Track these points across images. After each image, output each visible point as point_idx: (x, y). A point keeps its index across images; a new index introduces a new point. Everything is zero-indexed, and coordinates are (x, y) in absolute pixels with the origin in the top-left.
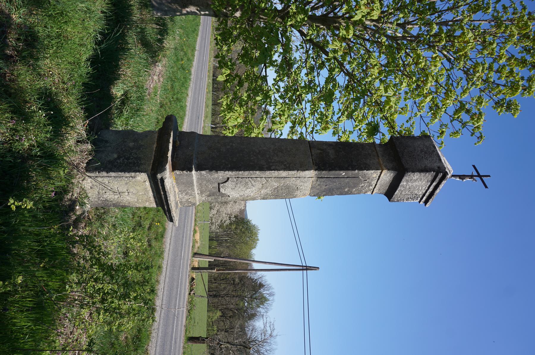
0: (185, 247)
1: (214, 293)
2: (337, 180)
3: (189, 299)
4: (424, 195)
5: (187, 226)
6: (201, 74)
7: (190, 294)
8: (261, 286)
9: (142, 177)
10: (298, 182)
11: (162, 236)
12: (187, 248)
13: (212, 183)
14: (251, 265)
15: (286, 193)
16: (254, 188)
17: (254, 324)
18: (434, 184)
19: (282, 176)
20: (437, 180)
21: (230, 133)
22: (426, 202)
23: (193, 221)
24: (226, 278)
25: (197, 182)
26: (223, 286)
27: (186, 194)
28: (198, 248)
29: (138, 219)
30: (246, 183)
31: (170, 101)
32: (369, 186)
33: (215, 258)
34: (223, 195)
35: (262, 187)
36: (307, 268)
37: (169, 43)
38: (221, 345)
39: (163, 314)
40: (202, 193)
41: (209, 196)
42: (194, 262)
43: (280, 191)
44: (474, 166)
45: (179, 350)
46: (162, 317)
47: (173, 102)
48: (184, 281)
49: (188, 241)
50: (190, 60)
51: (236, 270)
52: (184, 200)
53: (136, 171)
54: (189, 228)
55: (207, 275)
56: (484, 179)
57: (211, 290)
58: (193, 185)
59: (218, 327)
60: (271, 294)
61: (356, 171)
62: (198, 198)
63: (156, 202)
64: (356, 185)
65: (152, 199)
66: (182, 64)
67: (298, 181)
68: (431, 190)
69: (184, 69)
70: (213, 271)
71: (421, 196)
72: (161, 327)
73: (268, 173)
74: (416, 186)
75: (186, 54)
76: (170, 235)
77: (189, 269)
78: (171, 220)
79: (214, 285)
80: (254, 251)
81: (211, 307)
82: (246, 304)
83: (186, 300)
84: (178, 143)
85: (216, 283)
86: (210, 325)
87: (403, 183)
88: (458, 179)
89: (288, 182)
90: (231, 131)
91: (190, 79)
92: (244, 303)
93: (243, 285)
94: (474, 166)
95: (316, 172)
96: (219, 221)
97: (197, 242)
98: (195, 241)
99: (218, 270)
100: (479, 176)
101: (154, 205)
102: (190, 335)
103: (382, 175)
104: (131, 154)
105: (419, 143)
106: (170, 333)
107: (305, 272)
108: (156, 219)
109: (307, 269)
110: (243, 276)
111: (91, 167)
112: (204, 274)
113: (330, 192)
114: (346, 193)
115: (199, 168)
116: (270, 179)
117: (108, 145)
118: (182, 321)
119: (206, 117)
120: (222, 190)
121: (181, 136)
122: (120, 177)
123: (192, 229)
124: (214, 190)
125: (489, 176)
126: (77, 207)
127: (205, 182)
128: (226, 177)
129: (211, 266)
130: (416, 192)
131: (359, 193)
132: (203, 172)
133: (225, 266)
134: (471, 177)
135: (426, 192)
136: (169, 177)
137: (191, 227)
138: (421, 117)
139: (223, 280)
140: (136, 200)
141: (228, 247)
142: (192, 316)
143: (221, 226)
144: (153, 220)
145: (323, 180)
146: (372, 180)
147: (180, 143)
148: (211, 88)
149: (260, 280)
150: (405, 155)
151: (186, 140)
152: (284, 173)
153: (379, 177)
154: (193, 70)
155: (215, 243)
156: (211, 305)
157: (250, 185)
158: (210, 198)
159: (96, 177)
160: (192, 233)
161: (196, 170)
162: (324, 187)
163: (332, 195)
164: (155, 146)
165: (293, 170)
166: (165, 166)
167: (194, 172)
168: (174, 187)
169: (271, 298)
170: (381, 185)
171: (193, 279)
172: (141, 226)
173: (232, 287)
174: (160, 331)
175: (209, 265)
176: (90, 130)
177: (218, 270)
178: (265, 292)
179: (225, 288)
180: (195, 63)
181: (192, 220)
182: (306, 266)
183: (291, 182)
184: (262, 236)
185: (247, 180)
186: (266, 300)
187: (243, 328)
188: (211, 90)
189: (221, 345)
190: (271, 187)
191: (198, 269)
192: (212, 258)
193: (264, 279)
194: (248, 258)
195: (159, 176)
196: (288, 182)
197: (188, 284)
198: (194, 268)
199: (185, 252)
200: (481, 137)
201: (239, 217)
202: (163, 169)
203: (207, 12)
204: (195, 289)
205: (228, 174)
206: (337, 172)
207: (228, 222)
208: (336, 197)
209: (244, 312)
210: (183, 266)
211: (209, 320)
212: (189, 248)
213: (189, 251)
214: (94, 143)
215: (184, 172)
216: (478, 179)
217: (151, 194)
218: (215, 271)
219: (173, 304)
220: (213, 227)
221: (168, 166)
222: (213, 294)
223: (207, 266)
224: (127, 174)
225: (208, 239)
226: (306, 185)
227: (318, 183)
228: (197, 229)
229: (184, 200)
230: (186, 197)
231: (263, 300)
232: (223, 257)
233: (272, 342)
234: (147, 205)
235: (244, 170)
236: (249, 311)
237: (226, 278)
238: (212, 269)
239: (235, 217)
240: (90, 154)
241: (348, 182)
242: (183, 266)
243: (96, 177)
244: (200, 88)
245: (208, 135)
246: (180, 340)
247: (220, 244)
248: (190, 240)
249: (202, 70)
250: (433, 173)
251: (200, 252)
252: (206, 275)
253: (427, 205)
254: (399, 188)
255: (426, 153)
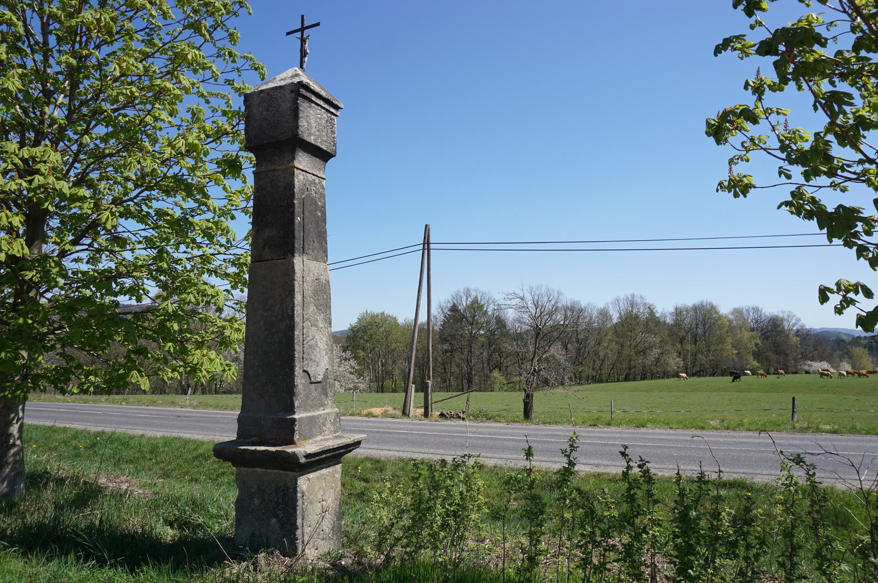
0: (394, 429)
1: (465, 381)
2: (306, 228)
3: (470, 420)
4: (328, 111)
5: (362, 427)
6: (96, 414)
7: (463, 419)
8: (454, 309)
9: (303, 483)
10: (309, 279)
11: (378, 461)
12: (395, 426)
13: (310, 392)
14: (422, 324)
15: (323, 292)
16: (317, 337)
17: (511, 319)
18: (314, 98)
19: (301, 301)
20: (308, 95)
21: (229, 370)
22: (337, 108)
23: (353, 418)
24: (443, 364)
25: (309, 411)
26: (455, 369)
27: (325, 425)
28: (395, 409)
29: (355, 495)
30: (310, 347)
31: (157, 463)
32: (315, 183)
33: (410, 383)
34: (326, 377)
35: (316, 326)
36: (427, 243)
37: (63, 468)
38: (535, 370)
39: (488, 455)
40: (322, 405)
41: (326, 395)
42: (417, 414)
43: (321, 302)
44: (288, 34)
45: (539, 430)
46: (492, 455)
47: (158, 458)
48: (444, 428)
49: (384, 425)
50: (76, 435)
51: (429, 350)
52: (332, 428)
53: (295, 492)
54: (364, 424)
55: (436, 394)
56: (306, 24)
57: (460, 387)
58: (313, 416)
59: (516, 375)
60: (468, 293)
61: (295, 202)
62: (329, 410)
63: (335, 464)
64: (314, 202)
65: (330, 469)
66: (85, 448)
67: (308, 278)
68: (321, 103)
69: (94, 445)
70: (430, 385)
71: (329, 115)
72: (504, 456)
73: (298, 319)
74: (316, 122)
75: (65, 443)
76: (376, 451)
77: (426, 422)
78: (357, 444)
79: (454, 383)
80: (401, 320)
81: (486, 386)
82: (482, 332)
83: (471, 424)
84: (254, 439)
85: (450, 380)
86: (511, 386)
87: (312, 139)
88: (306, 59)
89: (309, 292)
90: (227, 368)
91: (113, 433)
92: (480, 335)
93: (453, 336)
94: (288, 34)
95: (296, 255)
96: (352, 376)
97: (386, 411)
98: (385, 414)
99: (429, 379)
100: (302, 29)
101: (339, 467)
102: (521, 414)
103: (301, 167)
104: (271, 501)
105: (255, 111)
106: (514, 443)
107: (432, 246)
108: (353, 472)
109: (428, 243)
110: (440, 337)
111: (291, 551)
112: (434, 400)
113: (322, 236)
114: (324, 213)
115: (291, 409)
116: (306, 316)
117: (257, 533)
118: (501, 428)
119: (173, 403)
120: (319, 379)
121: (244, 435)
122: (303, 512)
123: (366, 419)
124: (320, 389)
125: (303, 16)
126: (343, 563)
127: (309, 402)
128: (303, 374)
129: (422, 388)
130: (324, 122)
131: (324, 197)
132: (296, 404)
133: (422, 366)
134: (303, 41)
135: (324, 108)
136: (304, 448)
137: (363, 421)
138: (203, 81)
139: (445, 369)
140: (332, 491)
141: (394, 362)
142: (496, 413)
143: (360, 374)
144: (354, 476)
145: (306, 246)
146: (307, 180)
147: (255, 436)
148: (117, 397)
149: (446, 311)
150: (274, 132)
151: (247, 428)
152: (298, 298)
153: (303, 171)
154: (94, 429)
155: (388, 383)
156: (483, 385)
157: (312, 342)
158: (330, 394)
159: (303, 542)
160: (372, 419)
161: (294, 413)
162: (316, 244)
163: (325, 232)
164: (259, 470)
165: (293, 286)
166: (289, 453)
167: (296, 416)
168: (316, 442)
169: (473, 294)
170: (314, 167)
171: (442, 415)
172: (363, 494)
173: (457, 355)
174: (510, 456)
175: (422, 391)
176: (238, 557)
177: (429, 379)
178: (464, 303)
179: (458, 366)
180: (79, 426)
181: (352, 421)
182: (424, 244)
183: (309, 288)
184: (376, 308)
185: (306, 346)
186: (475, 301)
187: (519, 337)
188: (121, 396)
189: (535, 370)
190: (315, 314)
191: (426, 408)
192: (410, 388)
193: (443, 304)
194: (412, 328)
195: (303, 460)
196: (309, 292)
197: (449, 422)
198: (426, 415)
199: (401, 429)
200: (240, 2)
201: (346, 345)
202: (294, 456)
203: (21, 407)
204: (457, 412)
205: (298, 371)
206: (296, 227)
207: (353, 362)
208: (329, 227)
209: (494, 335)
210: (422, 430)
211: (506, 388)
212: (394, 423)
213: (399, 423)
214: (256, 551)
215: (296, 428)
216: (306, 32)
217: (324, 471)
218: (430, 383)
219: (475, 442)
220: (362, 386)
221: (290, 449)
222: (466, 383)
223: (423, 394)
224: (300, 502)
225: (381, 395)
226: (312, 269)
227: (310, 252)
228: (365, 412)
229: (332, 428)
230: (328, 425)
231: (476, 306)
232: (410, 370)
233: (538, 293)
234: (338, 476)
235: (294, 350)
236: (493, 326)
237: (443, 364)
238: (427, 387)
239: (344, 351)
240: (272, 553)
241: (310, 212)
242: (422, 430)
243: (303, 542)
244: (123, 416)
245: (243, 402)
246: (526, 429)
247: (389, 374)
248: (382, 422)
249: (88, 414)
250: (300, 101)
251: (401, 406)
252: (435, 396)
253: (342, 106)
254: (319, 144)
255: (270, 105)
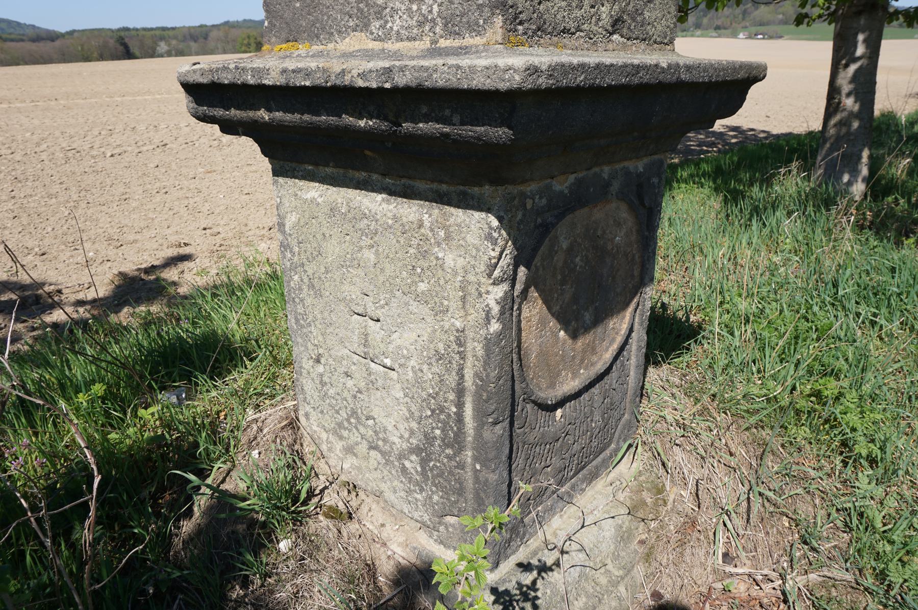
217: (375, 204)
